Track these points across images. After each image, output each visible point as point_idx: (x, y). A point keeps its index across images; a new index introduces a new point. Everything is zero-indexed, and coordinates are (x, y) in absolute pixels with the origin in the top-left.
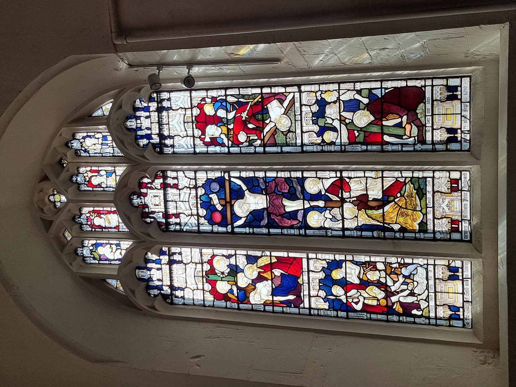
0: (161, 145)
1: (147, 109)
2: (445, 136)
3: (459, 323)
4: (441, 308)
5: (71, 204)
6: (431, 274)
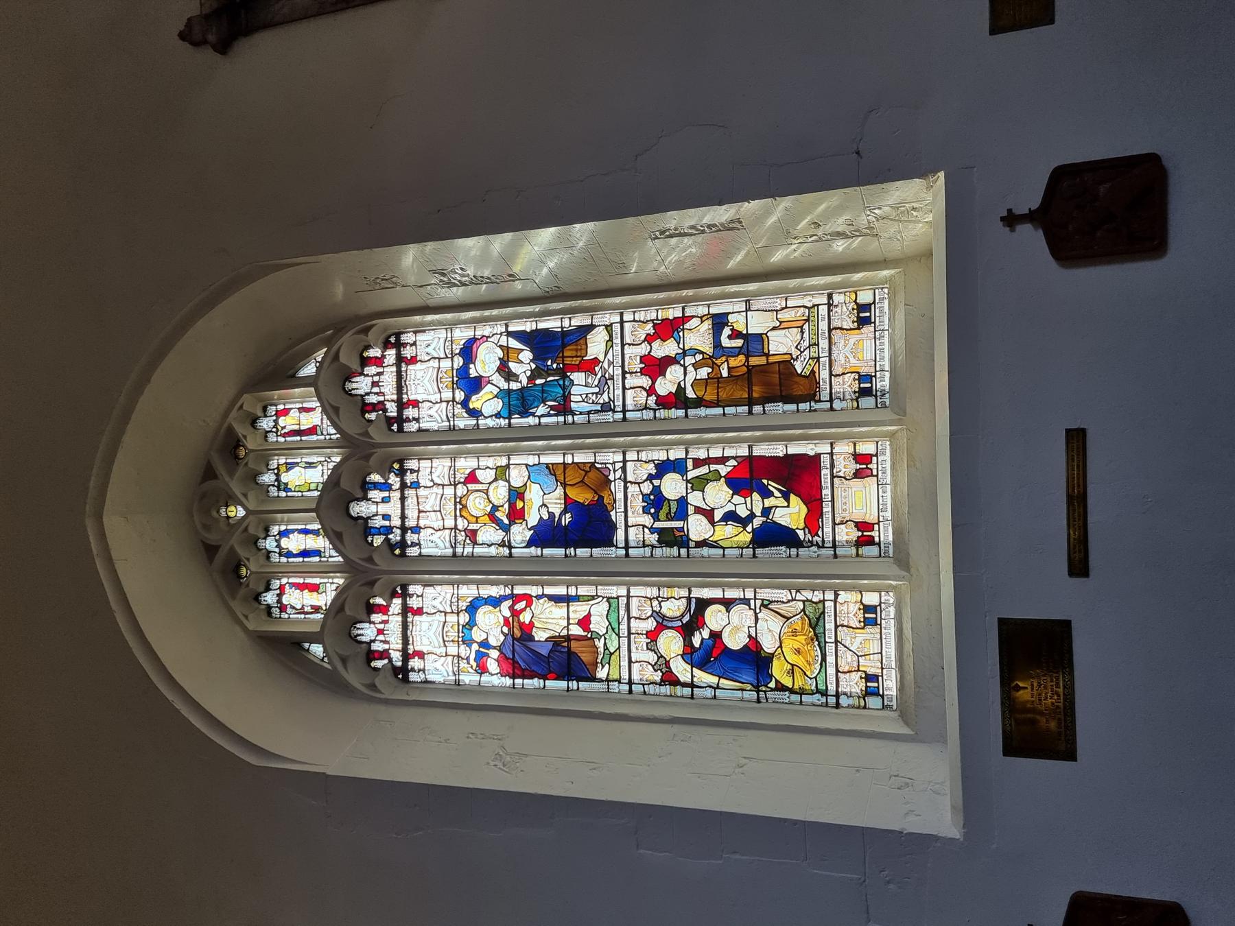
0: (401, 420)
1: (387, 487)
2: (855, 534)
3: (874, 550)
4: (843, 526)
5: (251, 518)
6: (830, 659)
